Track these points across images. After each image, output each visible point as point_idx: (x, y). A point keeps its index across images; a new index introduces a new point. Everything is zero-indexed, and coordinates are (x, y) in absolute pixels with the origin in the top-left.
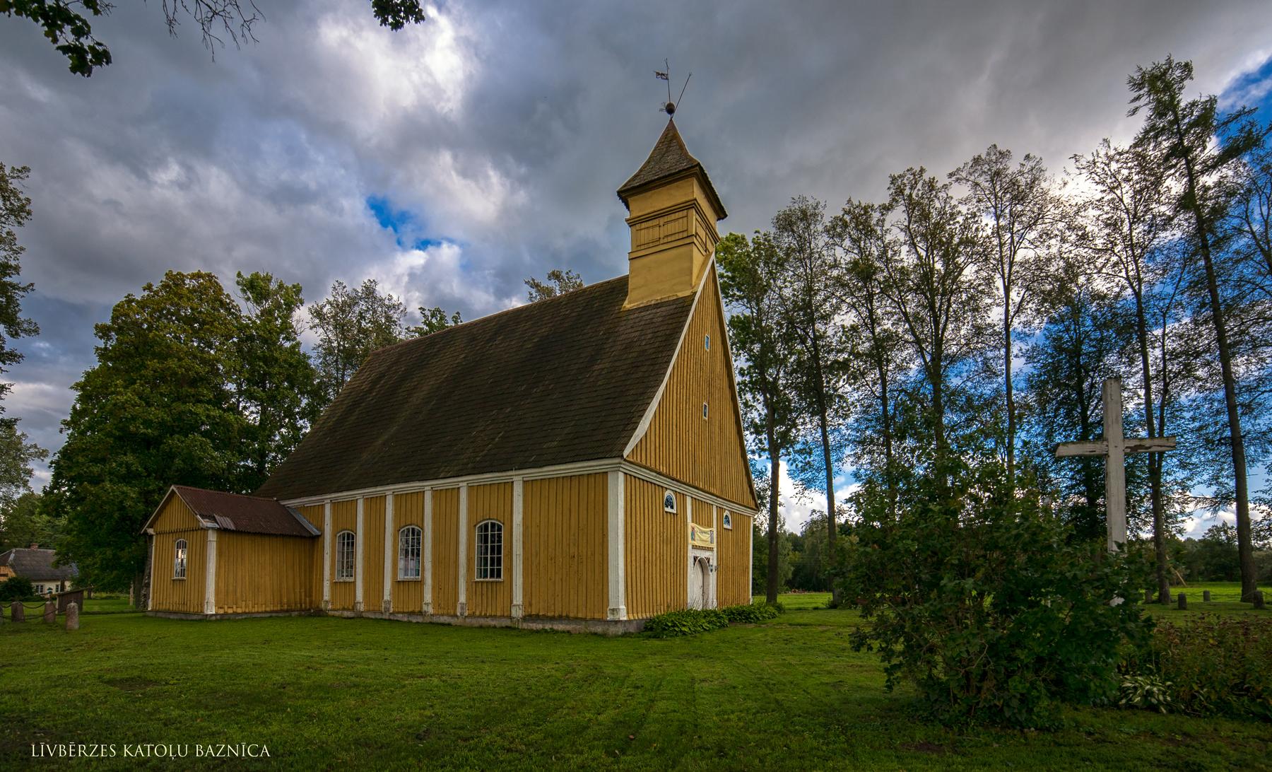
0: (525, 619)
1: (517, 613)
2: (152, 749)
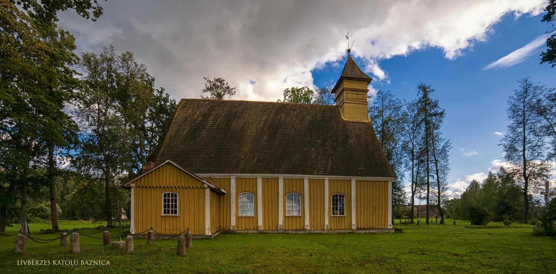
0: (358, 229)
1: (354, 227)
2: (64, 262)
